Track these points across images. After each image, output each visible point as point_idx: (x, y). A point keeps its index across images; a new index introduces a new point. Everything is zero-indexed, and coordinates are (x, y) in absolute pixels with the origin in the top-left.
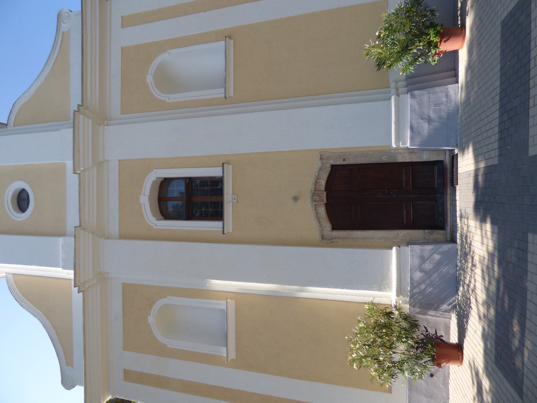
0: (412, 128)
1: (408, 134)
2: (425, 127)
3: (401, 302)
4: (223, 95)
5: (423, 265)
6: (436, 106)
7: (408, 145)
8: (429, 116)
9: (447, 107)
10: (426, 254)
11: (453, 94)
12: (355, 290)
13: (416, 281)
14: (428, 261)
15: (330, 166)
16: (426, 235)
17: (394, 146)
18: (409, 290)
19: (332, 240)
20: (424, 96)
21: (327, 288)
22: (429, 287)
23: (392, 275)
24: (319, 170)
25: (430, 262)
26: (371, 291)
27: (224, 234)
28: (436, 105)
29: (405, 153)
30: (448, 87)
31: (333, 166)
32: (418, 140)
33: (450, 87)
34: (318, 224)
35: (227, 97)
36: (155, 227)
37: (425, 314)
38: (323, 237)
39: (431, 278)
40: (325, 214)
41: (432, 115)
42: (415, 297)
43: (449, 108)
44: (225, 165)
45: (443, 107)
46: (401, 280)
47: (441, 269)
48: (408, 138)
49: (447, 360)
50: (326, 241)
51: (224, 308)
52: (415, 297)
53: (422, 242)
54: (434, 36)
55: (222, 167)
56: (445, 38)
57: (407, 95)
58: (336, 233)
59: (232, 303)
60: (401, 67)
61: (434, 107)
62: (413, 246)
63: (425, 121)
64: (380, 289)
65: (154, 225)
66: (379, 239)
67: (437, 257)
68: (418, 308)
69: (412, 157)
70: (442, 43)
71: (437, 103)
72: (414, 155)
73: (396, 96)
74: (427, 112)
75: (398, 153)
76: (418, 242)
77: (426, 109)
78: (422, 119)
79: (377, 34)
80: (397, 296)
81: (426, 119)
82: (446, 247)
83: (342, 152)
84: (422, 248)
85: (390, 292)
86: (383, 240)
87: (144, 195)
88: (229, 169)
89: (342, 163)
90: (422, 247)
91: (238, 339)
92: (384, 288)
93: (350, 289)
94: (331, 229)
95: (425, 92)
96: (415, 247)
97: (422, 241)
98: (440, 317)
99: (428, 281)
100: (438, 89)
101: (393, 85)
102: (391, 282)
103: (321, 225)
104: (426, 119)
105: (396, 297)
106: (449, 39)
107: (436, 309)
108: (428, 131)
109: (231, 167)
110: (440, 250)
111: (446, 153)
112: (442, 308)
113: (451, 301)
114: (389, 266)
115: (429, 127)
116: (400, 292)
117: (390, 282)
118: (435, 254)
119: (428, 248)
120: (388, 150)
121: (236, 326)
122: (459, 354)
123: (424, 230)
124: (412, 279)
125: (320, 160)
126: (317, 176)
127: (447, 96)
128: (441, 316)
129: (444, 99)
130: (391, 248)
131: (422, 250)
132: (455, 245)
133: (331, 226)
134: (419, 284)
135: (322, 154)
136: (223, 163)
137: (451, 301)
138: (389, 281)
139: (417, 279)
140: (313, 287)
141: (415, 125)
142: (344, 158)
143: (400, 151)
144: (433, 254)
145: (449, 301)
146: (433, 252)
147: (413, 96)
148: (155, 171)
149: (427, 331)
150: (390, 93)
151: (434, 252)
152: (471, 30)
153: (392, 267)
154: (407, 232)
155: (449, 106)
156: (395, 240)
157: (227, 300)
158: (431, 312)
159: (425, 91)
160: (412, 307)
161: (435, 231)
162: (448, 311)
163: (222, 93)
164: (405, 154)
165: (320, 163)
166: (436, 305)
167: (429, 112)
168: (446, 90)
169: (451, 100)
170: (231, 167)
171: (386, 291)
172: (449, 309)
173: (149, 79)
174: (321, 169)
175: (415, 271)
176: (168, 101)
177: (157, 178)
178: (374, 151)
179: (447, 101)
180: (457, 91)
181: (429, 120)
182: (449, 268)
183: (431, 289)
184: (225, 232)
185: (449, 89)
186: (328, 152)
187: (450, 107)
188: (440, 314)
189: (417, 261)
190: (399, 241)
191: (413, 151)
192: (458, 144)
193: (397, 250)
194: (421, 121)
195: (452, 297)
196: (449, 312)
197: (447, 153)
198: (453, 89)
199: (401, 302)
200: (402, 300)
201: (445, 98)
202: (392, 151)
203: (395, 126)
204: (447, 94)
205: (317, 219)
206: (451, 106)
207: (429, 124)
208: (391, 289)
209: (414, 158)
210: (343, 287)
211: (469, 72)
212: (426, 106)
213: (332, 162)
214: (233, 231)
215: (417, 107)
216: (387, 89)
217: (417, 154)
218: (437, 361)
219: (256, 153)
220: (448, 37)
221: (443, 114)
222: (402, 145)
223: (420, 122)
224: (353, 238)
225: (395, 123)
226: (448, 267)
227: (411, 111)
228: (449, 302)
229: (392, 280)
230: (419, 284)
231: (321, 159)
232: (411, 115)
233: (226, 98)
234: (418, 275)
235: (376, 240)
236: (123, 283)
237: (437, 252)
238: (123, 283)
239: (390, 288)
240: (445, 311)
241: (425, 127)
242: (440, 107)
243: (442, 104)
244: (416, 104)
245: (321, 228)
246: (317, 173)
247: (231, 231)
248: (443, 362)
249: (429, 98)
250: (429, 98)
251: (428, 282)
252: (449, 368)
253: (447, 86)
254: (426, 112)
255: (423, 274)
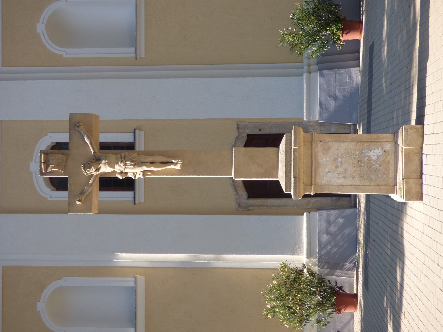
0: (321, 104)
1: (318, 109)
2: (332, 104)
3: (311, 265)
4: (133, 55)
5: (329, 228)
6: (341, 86)
7: (317, 119)
8: (336, 95)
9: (350, 88)
10: (332, 218)
11: (355, 76)
12: (270, 255)
13: (324, 243)
14: (333, 225)
15: (247, 135)
16: (333, 202)
17: (305, 120)
18: (317, 251)
19: (248, 208)
20: (331, 75)
21: (243, 254)
22: (334, 248)
23: (303, 239)
24: (236, 140)
25: (335, 225)
26: (285, 255)
27: (135, 204)
28: (341, 85)
29: (315, 126)
30: (351, 69)
31: (249, 135)
32: (325, 115)
33: (352, 70)
34: (235, 193)
35: (138, 58)
36: (49, 199)
37: (333, 275)
38: (239, 205)
39: (336, 240)
40: (241, 182)
41: (338, 94)
42: (322, 258)
43: (352, 88)
44: (137, 131)
45: (347, 87)
46: (310, 243)
47: (344, 231)
48: (317, 113)
49: (345, 306)
50: (242, 209)
51: (132, 286)
52: (322, 258)
53: (331, 208)
54: (336, 30)
55: (132, 134)
56: (347, 31)
57: (317, 73)
58: (252, 201)
59: (141, 279)
60: (310, 52)
61: (339, 86)
62: (321, 211)
63: (332, 98)
64: (292, 253)
65: (48, 197)
66: (292, 206)
67: (341, 220)
68: (327, 268)
69: (322, 130)
70: (344, 35)
71: (342, 83)
72: (324, 128)
73: (308, 74)
74: (334, 90)
75: (310, 125)
76: (326, 208)
77: (333, 88)
78: (330, 97)
79: (291, 17)
80: (308, 257)
81: (333, 97)
82: (348, 211)
83: (258, 123)
84: (328, 213)
85: (301, 255)
86: (295, 207)
87: (35, 162)
88: (141, 135)
89: (258, 133)
90: (329, 212)
91: (148, 317)
92: (296, 252)
93: (265, 255)
94: (247, 197)
95: (332, 72)
96: (322, 212)
97: (330, 208)
98: (345, 276)
99: (333, 243)
100: (342, 71)
101: (305, 61)
102: (302, 246)
103: (237, 193)
104: (333, 97)
105: (307, 259)
106: (350, 32)
107: (341, 268)
108: (334, 108)
109: (142, 133)
110: (343, 214)
111: (351, 127)
112: (346, 267)
113: (352, 259)
114: (301, 231)
115: (335, 105)
116: (309, 255)
117: (301, 246)
118: (339, 218)
119: (334, 212)
120: (301, 122)
121: (146, 304)
122: (354, 300)
123: (332, 198)
124: (320, 241)
125: (237, 129)
126: (234, 145)
127: (350, 77)
128: (346, 276)
129: (348, 80)
130: (303, 214)
131: (328, 215)
132: (355, 209)
133: (247, 194)
134: (326, 246)
135: (239, 123)
136: (135, 129)
137: (352, 259)
138: (300, 245)
139: (324, 241)
140: (230, 254)
141: (323, 102)
142: (259, 128)
143: (311, 123)
144: (338, 217)
145: (350, 259)
146: (338, 216)
147: (322, 75)
148: (49, 134)
149: (330, 283)
150: (303, 68)
151: (339, 216)
152: (365, 25)
153: (303, 231)
154: (317, 199)
155: (351, 87)
156: (307, 207)
157: (137, 276)
158: (338, 272)
159: (332, 71)
160: (321, 268)
161: (341, 198)
162: (351, 270)
163: (132, 53)
164: (316, 127)
165: (236, 132)
166: (341, 264)
167: (335, 91)
168: (350, 72)
169: (353, 81)
170: (142, 133)
171: (298, 255)
172: (352, 267)
173: (41, 28)
174: (237, 138)
175: (323, 234)
176: (65, 56)
177: (52, 143)
178: (289, 122)
179: (350, 82)
180: (358, 74)
181: (335, 98)
182: (350, 229)
183: (336, 249)
184: (137, 202)
185: (352, 71)
186: (245, 122)
187: (353, 88)
188: (345, 273)
189: (324, 225)
190: (310, 208)
191: (324, 124)
192: (358, 121)
193: (307, 215)
194: (329, 98)
195: (353, 255)
196: (352, 271)
197: (352, 127)
198: (355, 72)
199: (311, 265)
200: (312, 262)
201: (349, 79)
202: (304, 123)
203: (307, 101)
204: (350, 76)
205: (233, 187)
206: (353, 87)
207: (335, 102)
208: (302, 252)
209: (324, 131)
210: (259, 253)
211: (363, 63)
212: (333, 85)
213: (248, 132)
214: (144, 201)
215: (325, 86)
216: (301, 63)
217: (326, 127)
218: (338, 308)
219: (171, 120)
220: (348, 31)
221: (347, 93)
222: (312, 119)
223: (328, 99)
224: (267, 206)
225: (306, 99)
226: (349, 229)
227: (320, 88)
228: (350, 261)
229: (303, 244)
230: (326, 246)
231: (238, 128)
232: (320, 92)
233: (136, 59)
234: (325, 237)
235: (289, 207)
236: (3, 266)
237: (341, 216)
238: (3, 266)
239: (301, 251)
240: (349, 270)
241: (332, 104)
242: (345, 87)
243: (347, 84)
244: (324, 82)
245: (238, 196)
246: (234, 142)
247: (142, 201)
248: (342, 308)
249: (336, 78)
250: (336, 78)
251: (333, 243)
252: (353, 324)
253: (351, 69)
254: (333, 91)
255: (329, 236)
